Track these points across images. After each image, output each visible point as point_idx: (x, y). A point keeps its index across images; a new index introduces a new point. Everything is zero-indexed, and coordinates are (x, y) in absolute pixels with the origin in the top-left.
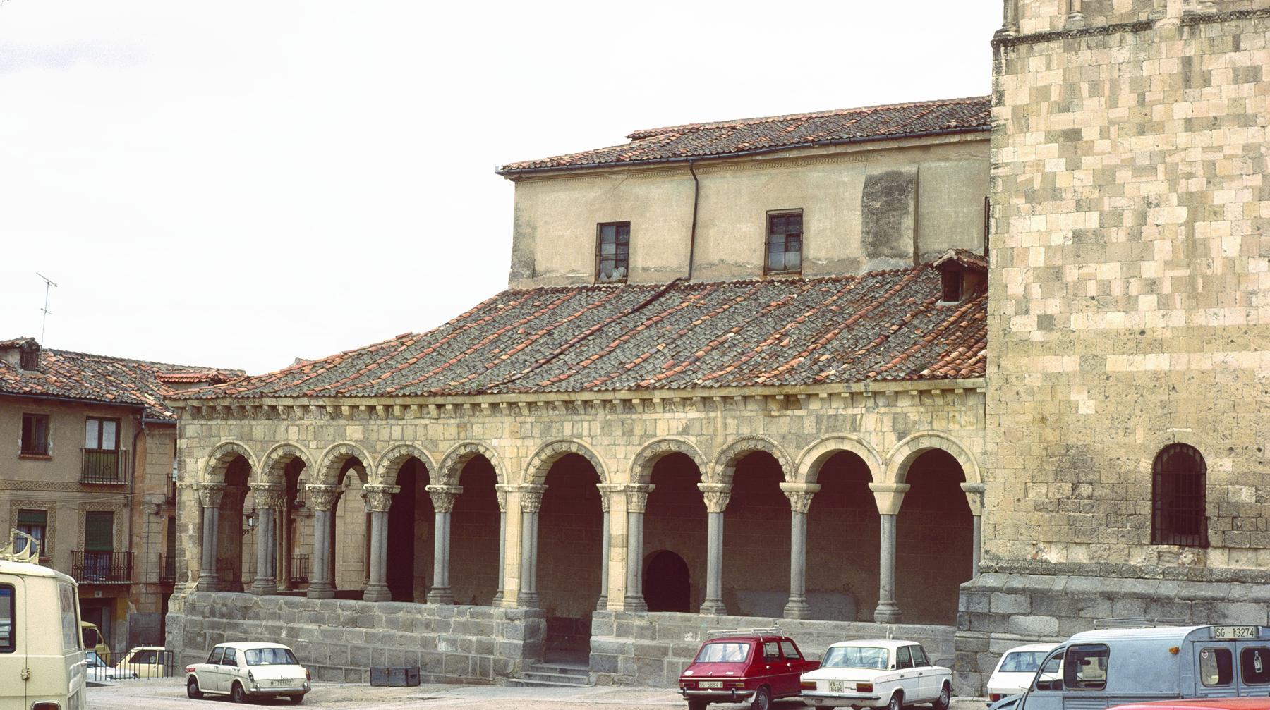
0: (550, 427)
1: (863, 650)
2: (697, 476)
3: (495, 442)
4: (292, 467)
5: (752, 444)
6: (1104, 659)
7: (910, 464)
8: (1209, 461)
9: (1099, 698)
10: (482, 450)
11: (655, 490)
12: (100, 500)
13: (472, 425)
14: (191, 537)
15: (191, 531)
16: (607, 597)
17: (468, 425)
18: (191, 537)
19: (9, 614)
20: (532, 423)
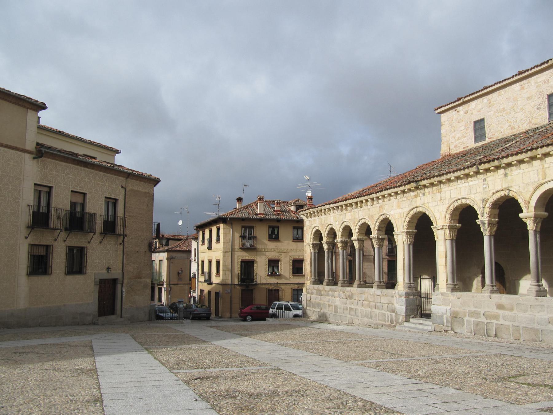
0: (412, 201)
1: (171, 242)
2: (476, 216)
3: (392, 212)
4: (348, 231)
5: (459, 202)
6: (36, 210)
7: (549, 197)
8: (458, 214)
9: (124, 222)
10: (388, 216)
11: (461, 227)
12: (247, 256)
13: (384, 206)
14: (308, 263)
15: (308, 262)
16: (350, 281)
17: (383, 206)
18: (308, 263)
19: (21, 110)
20: (405, 201)
